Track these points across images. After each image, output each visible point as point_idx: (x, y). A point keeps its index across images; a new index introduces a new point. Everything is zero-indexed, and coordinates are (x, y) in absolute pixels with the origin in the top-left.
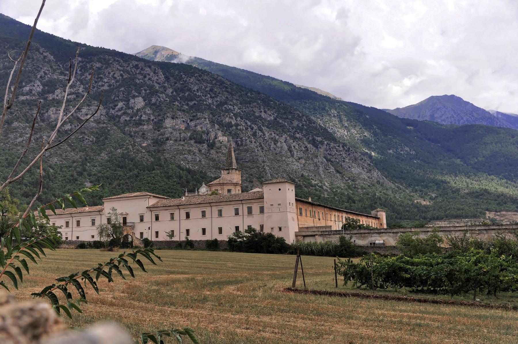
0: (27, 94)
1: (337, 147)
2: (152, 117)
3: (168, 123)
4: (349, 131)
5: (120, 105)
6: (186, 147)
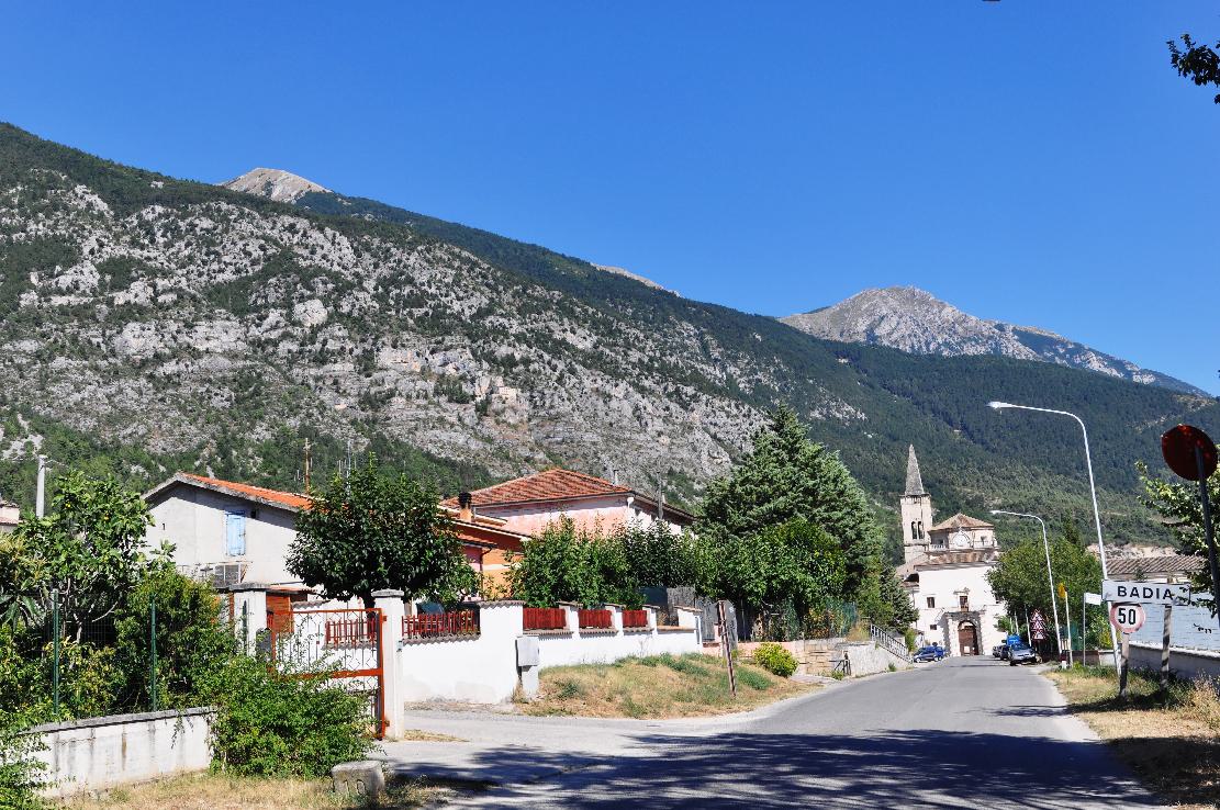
0: (69, 291)
1: (726, 408)
2: (349, 345)
3: (386, 357)
4: (724, 369)
5: (274, 316)
6: (432, 412)
